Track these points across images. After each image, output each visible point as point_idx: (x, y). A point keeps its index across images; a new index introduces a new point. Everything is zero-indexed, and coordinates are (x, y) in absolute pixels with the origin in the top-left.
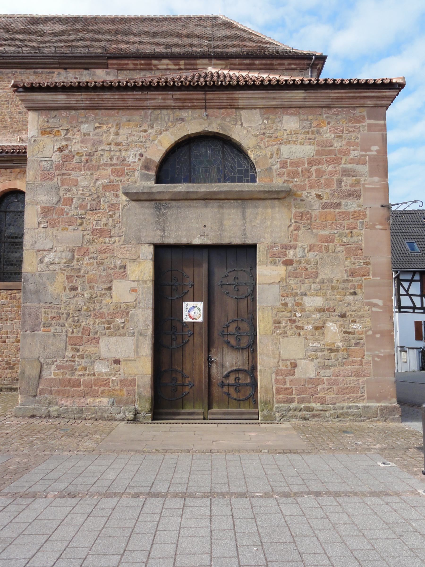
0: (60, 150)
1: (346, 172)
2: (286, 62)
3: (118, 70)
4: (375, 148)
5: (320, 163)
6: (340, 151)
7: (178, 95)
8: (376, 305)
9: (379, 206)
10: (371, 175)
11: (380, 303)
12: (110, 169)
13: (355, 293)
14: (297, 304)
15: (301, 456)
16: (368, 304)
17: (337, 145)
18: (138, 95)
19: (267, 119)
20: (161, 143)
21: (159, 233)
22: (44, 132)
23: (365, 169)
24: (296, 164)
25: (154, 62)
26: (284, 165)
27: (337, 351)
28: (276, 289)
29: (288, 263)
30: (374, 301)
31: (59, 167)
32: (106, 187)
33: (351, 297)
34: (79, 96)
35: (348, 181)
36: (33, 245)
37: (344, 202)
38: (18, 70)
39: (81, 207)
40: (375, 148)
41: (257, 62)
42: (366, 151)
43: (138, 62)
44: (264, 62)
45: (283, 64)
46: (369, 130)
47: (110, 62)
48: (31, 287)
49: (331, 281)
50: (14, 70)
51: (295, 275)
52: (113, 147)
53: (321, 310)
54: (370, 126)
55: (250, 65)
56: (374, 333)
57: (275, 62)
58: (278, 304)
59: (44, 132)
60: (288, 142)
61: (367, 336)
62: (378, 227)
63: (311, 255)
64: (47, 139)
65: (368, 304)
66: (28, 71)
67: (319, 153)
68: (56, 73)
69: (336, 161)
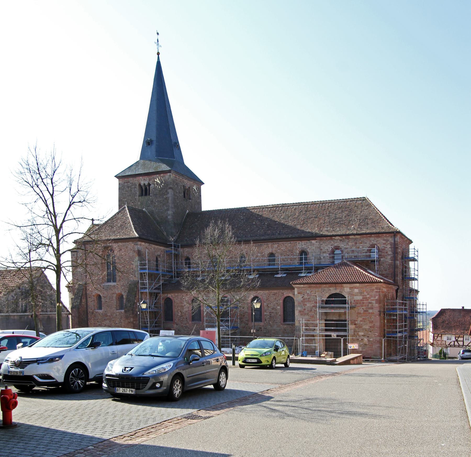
0: (302, 297)
1: (370, 303)
2: (384, 235)
3: (320, 240)
4: (377, 297)
5: (364, 301)
6: (368, 298)
7: (329, 285)
8: (376, 335)
9: (377, 311)
10: (376, 304)
11: (377, 334)
12: (314, 302)
13: (371, 332)
14: (357, 334)
15: (60, 239)
16: (374, 334)
17: (368, 296)
18: (320, 285)
19: (351, 290)
20: (325, 296)
21: (325, 317)
22: (299, 293)
23: (374, 302)
24: (357, 301)
25: (333, 237)
26: (354, 301)
27: (366, 345)
28: (353, 331)
29: (355, 324)
30: (376, 334)
31: (302, 301)
32: (313, 306)
33: (370, 333)
34: (306, 285)
35: (370, 305)
36: (297, 319)
37: (369, 310)
38: (284, 242)
39: (308, 311)
40: (377, 297)
41: (373, 235)
42: (375, 298)
43: (327, 238)
44: (375, 235)
45: (383, 235)
46: (376, 293)
47: (317, 238)
48: (297, 328)
49: (365, 329)
50: (283, 242)
51: (356, 327)
52: (314, 297)
53: (363, 335)
54: (376, 291)
55: (370, 236)
56: (375, 341)
57: (380, 235)
58: (353, 334)
59: (299, 293)
60: (356, 296)
61: (374, 342)
62: (377, 316)
63: (361, 323)
64: (299, 295)
65: (374, 334)
66: (288, 242)
67: (363, 298)
68: (298, 243)
69: (368, 300)
